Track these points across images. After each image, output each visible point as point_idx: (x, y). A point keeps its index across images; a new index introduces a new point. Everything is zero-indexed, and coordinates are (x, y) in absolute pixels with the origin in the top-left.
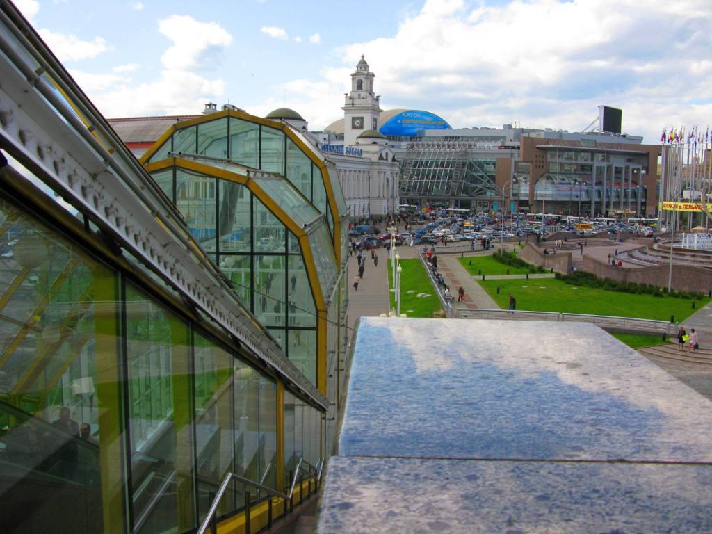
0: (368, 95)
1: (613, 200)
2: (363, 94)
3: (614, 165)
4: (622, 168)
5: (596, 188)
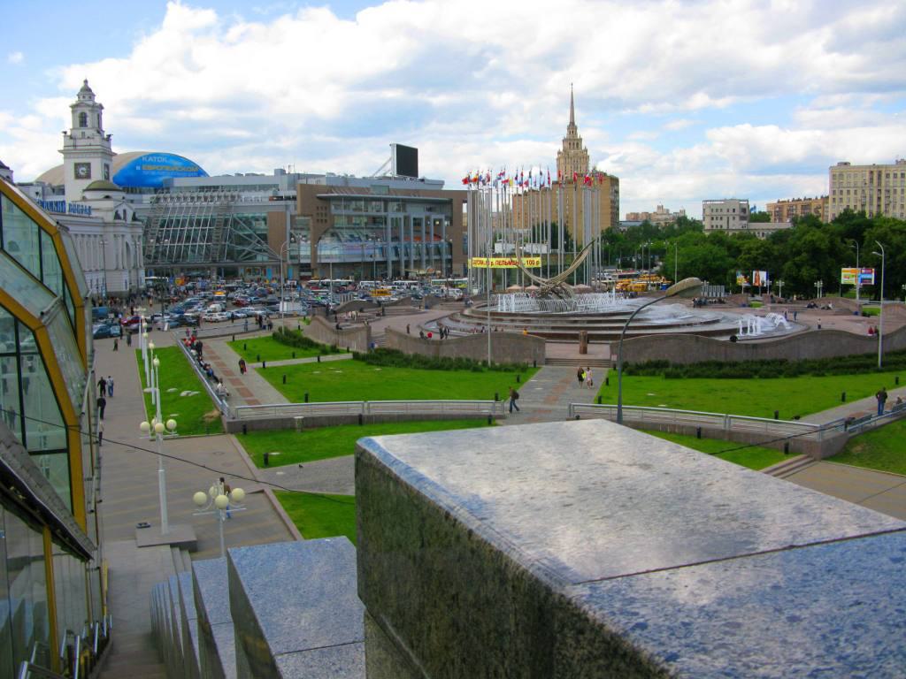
0: (95, 133)
1: (413, 258)
2: (89, 132)
4: (421, 219)
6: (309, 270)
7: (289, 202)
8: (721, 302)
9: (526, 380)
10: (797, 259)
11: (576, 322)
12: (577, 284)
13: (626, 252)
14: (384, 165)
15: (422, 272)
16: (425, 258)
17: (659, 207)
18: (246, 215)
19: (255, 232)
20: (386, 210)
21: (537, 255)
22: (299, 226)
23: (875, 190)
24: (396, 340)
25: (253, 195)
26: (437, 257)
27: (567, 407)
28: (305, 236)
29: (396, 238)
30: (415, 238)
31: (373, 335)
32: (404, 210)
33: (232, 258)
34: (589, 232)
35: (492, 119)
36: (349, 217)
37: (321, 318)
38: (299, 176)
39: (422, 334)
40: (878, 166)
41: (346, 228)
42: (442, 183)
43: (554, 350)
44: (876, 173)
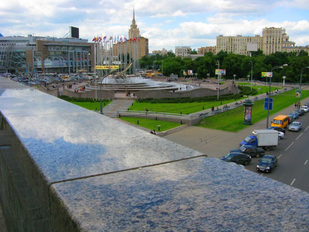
3: (77, 51)
4: (80, 53)
5: (70, 61)
6: (41, 70)
7: (33, 46)
8: (176, 80)
9: (107, 105)
10: (202, 66)
11: (127, 86)
12: (131, 74)
13: (150, 64)
14: (67, 34)
15: (80, 71)
16: (82, 66)
17: (163, 49)
18: (18, 51)
20: (68, 49)
21: (117, 65)
22: (37, 55)
23: (231, 45)
24: (67, 93)
25: (20, 44)
26: (86, 66)
27: (117, 112)
28: (39, 58)
29: (71, 59)
30: (78, 59)
31: (59, 91)
32: (74, 49)
33: (13, 66)
34: (137, 57)
35: (107, 19)
36: (55, 52)
37: (43, 86)
38: (37, 37)
39: (75, 91)
40: (231, 37)
41: (54, 56)
42: (87, 40)
43: (117, 95)
44: (231, 39)
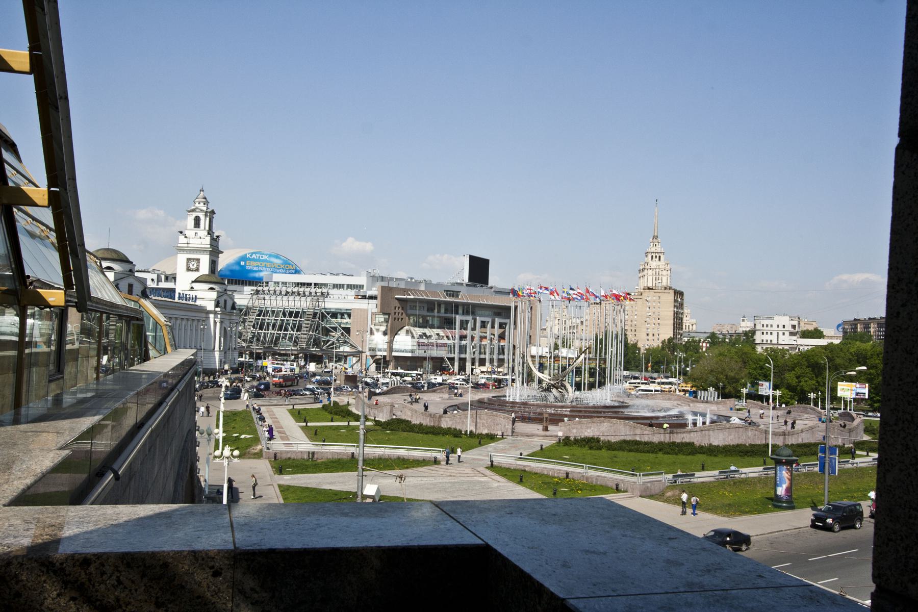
19: (340, 326)
